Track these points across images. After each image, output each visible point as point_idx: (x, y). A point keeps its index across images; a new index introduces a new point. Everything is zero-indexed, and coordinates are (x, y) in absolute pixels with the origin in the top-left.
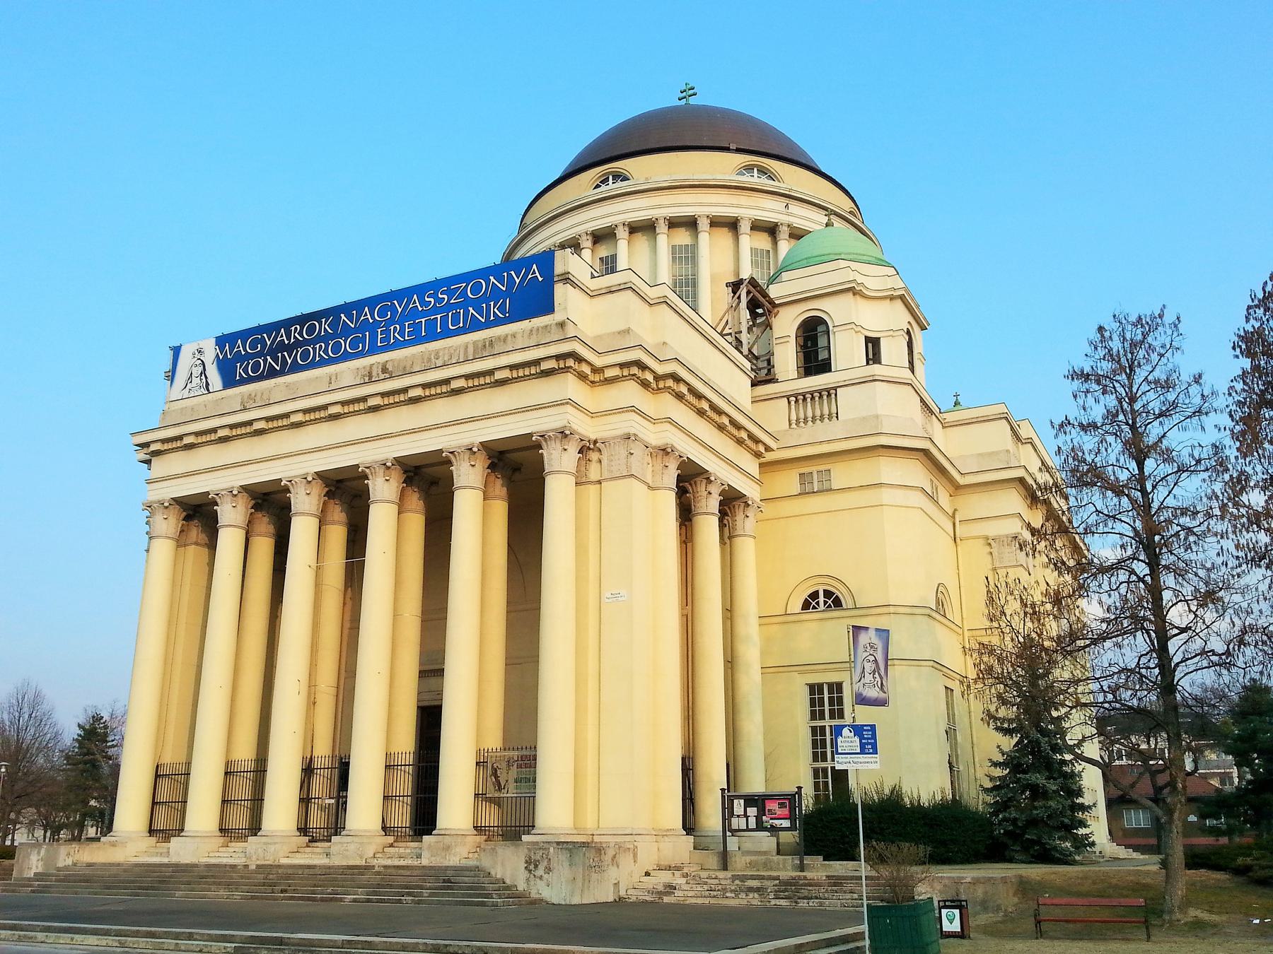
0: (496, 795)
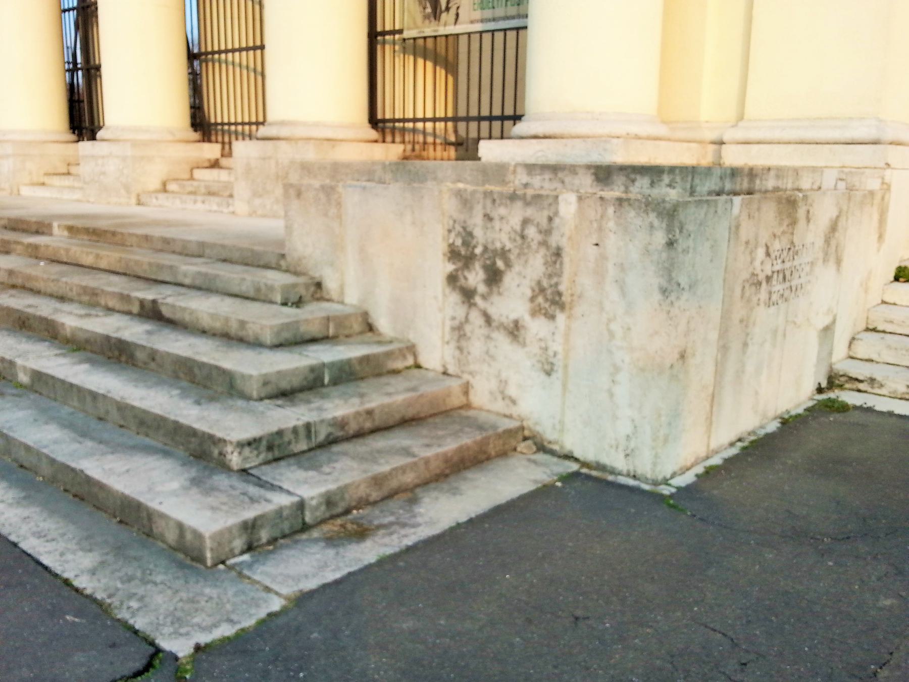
0: (428, 31)
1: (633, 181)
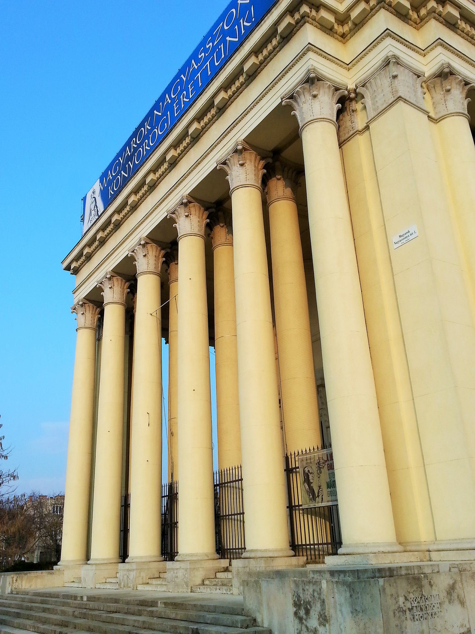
0: (312, 506)
1: (340, 575)
